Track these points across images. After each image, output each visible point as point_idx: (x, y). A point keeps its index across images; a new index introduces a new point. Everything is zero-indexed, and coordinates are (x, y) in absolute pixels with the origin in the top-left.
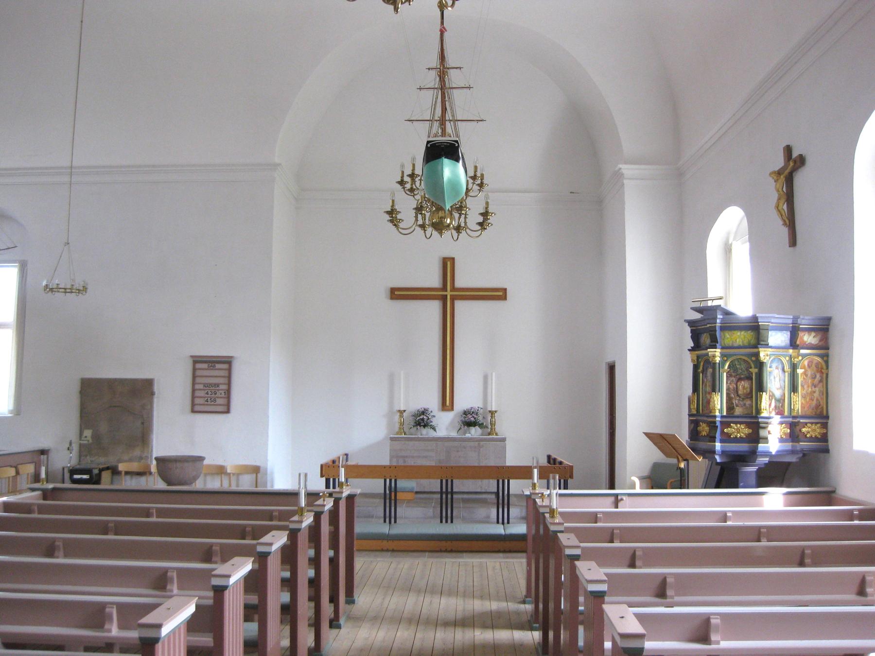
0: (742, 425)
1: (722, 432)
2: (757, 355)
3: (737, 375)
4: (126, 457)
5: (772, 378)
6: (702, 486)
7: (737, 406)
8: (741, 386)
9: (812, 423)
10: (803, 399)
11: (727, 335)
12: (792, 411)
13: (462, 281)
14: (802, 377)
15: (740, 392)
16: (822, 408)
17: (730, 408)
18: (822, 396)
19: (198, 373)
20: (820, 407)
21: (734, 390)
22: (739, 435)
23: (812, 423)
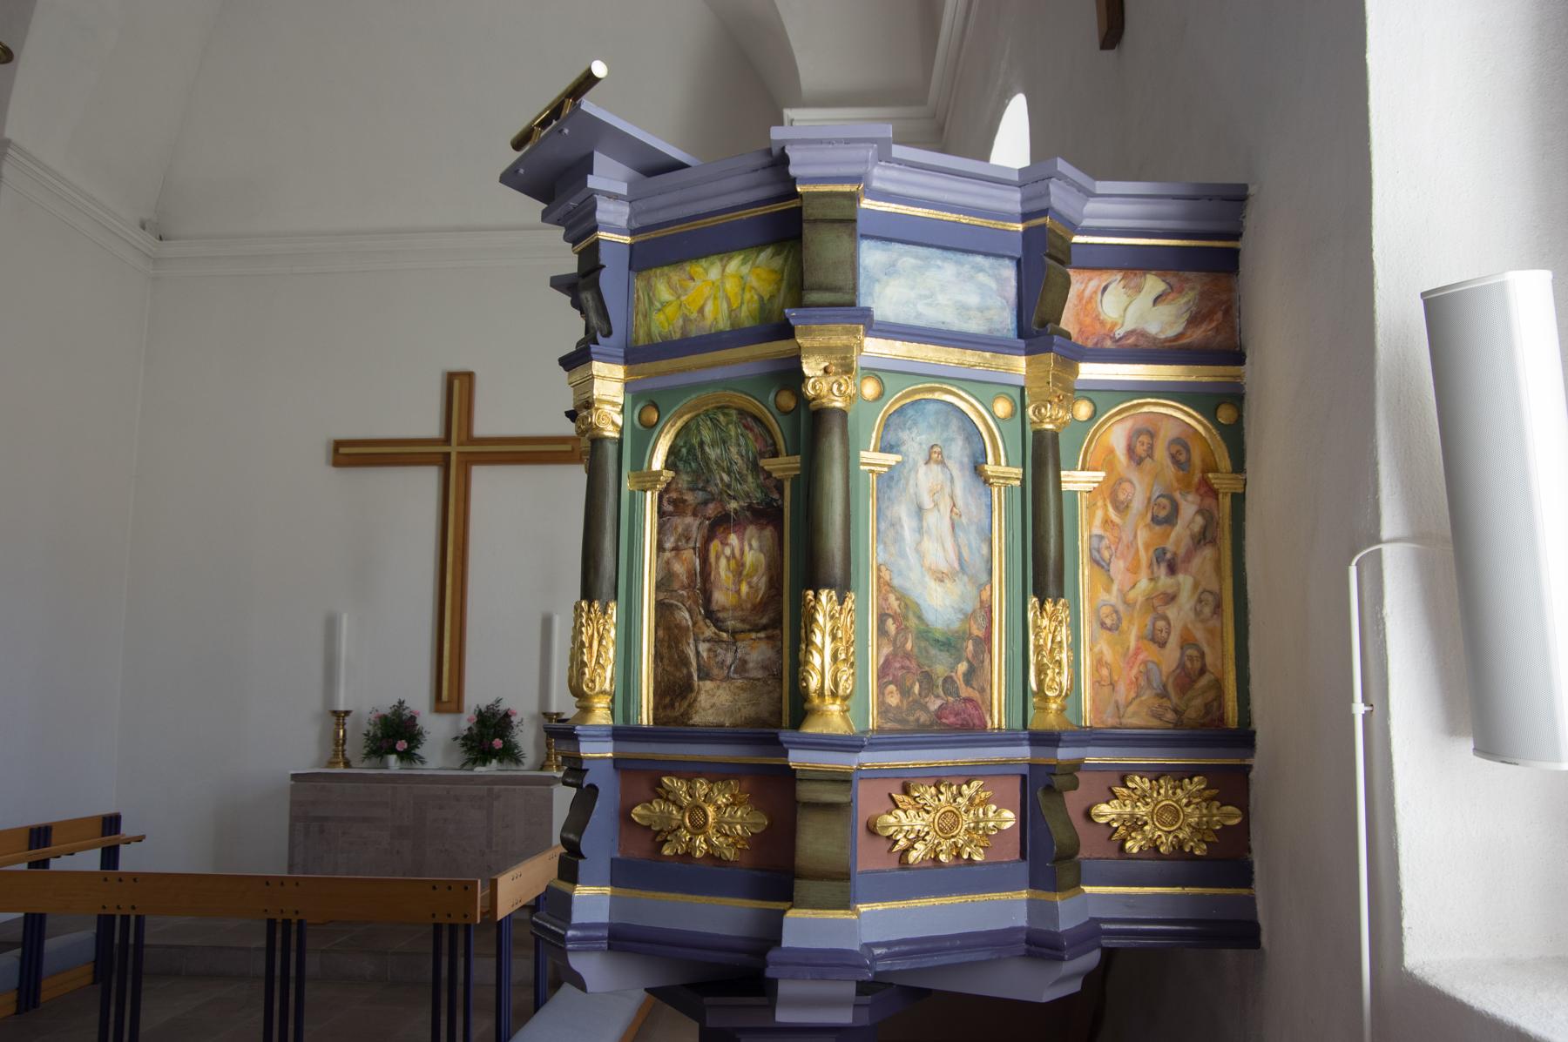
2: (791, 375)
3: (705, 503)
6: (1079, 893)
7: (705, 675)
8: (723, 562)
9: (1156, 774)
10: (1106, 634)
11: (663, 286)
12: (1032, 701)
13: (486, 424)
14: (1099, 514)
15: (720, 598)
16: (1218, 685)
17: (673, 690)
18: (1214, 622)
21: (690, 586)
22: (700, 841)
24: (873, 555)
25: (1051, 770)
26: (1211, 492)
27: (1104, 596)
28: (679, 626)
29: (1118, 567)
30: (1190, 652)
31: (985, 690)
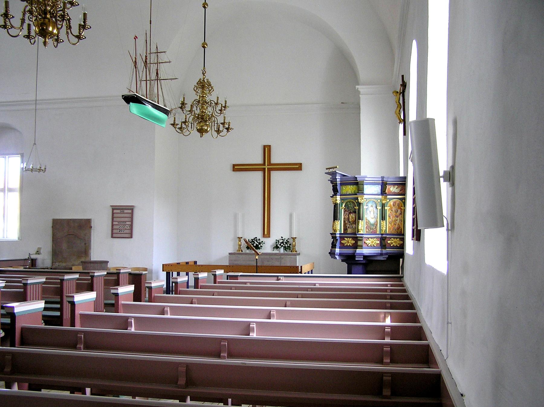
0: (350, 239)
1: (341, 243)
2: (357, 199)
4: (76, 263)
5: (368, 212)
7: (349, 228)
9: (394, 238)
12: (381, 231)
13: (275, 159)
14: (389, 211)
15: (350, 220)
16: (401, 229)
17: (345, 229)
19: (115, 215)
20: (400, 229)
22: (348, 244)
23: (394, 238)
24: (365, 216)
25: (383, 237)
26: (401, 209)
27: (390, 220)
28: (346, 223)
29: (391, 217)
30: (399, 226)
31: (377, 230)
